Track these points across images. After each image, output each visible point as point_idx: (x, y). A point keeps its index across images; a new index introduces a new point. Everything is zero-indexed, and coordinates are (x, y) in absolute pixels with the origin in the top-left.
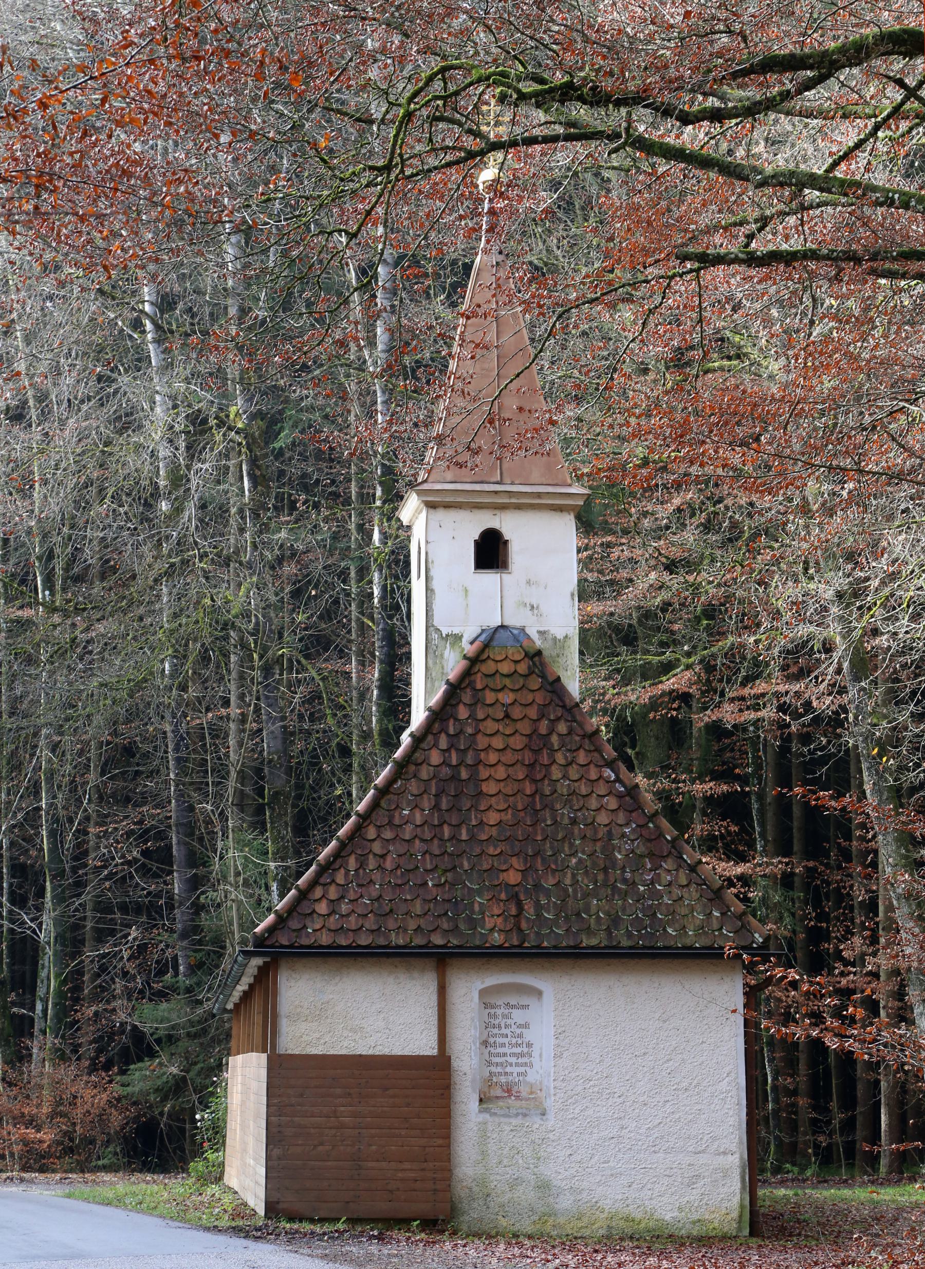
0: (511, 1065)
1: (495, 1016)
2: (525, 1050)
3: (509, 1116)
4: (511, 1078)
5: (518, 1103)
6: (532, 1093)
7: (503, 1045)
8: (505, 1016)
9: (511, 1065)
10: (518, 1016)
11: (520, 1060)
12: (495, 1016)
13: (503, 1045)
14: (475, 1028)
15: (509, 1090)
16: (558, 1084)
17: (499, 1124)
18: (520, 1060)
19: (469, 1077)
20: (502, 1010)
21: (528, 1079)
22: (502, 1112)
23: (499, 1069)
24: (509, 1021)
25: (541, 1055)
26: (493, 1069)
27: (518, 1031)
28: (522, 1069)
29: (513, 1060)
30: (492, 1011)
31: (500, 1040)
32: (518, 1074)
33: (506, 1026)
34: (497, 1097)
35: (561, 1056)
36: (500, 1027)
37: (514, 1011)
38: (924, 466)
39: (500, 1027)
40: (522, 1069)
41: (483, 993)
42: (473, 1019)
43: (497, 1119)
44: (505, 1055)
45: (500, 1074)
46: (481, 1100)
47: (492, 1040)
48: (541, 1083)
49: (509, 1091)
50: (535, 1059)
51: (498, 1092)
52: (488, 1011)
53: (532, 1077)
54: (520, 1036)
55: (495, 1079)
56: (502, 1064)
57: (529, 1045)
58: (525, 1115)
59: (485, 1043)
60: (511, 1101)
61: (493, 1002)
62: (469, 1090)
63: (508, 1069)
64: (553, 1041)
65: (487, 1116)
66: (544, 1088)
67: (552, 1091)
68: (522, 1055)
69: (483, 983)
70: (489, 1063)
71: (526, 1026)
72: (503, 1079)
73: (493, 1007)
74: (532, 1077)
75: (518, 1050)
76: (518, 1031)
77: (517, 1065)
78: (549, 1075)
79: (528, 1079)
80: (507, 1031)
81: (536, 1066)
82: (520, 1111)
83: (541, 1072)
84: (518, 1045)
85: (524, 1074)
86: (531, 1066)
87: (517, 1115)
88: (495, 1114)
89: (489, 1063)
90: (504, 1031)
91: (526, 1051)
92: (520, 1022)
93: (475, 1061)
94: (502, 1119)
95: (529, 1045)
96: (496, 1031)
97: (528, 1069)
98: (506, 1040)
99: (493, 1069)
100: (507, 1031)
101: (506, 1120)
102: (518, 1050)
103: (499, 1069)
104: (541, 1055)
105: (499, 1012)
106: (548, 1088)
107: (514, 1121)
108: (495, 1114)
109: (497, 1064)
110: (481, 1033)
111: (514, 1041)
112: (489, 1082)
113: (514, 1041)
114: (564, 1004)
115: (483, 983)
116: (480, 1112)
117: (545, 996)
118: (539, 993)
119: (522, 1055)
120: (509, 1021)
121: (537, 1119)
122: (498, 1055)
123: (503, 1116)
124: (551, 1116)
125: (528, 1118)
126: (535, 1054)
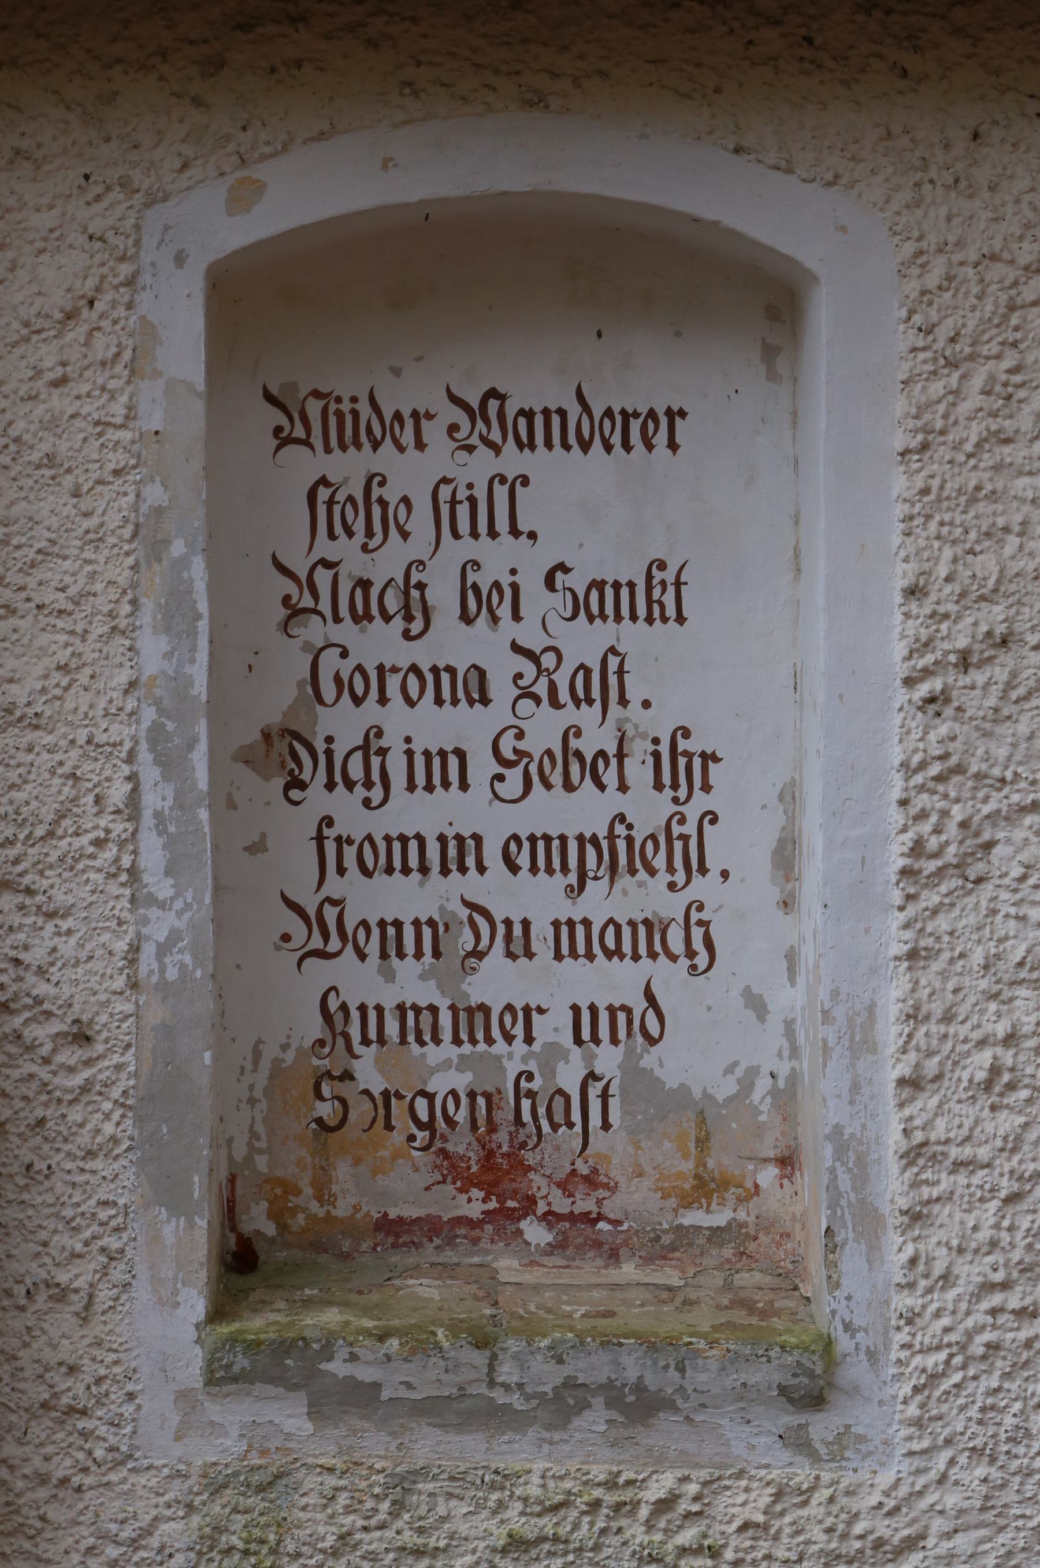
0: (518, 942)
1: (375, 512)
2: (648, 809)
3: (492, 1418)
4: (514, 1058)
5: (581, 1288)
6: (705, 1188)
7: (444, 769)
8: (457, 512)
9: (518, 942)
10: (583, 509)
11: (598, 903)
12: (375, 512)
13: (444, 769)
14: (175, 616)
15: (497, 1165)
16: (948, 1115)
17: (401, 1487)
18: (598, 903)
19: (119, 1065)
20: (439, 458)
21: (673, 1063)
22: (428, 1380)
23: (413, 983)
24: (497, 558)
25: (786, 857)
26: (358, 981)
27: (584, 643)
28: (615, 982)
29: (537, 899)
30: (349, 469)
31: (434, 725)
32: (586, 1025)
33: (477, 602)
34: (393, 1230)
35: (968, 869)
36: (414, 610)
37: (535, 463)
38: (366, 1566)
39: (414, 610)
40: (615, 982)
41: (245, 298)
42: (147, 533)
43: (376, 1446)
44: (461, 853)
45: (418, 1023)
46: (241, 1265)
47: (342, 725)
48: (787, 1097)
49: (499, 1175)
50: (736, 894)
51: (407, 1186)
52: (305, 465)
53: (705, 1048)
54: (603, 684)
55: (369, 1072)
56: (434, 931)
57: (683, 766)
58: (638, 1406)
59: (285, 754)
60: (521, 1266)
61: (347, 384)
62: (120, 1180)
63: (496, 982)
64: (897, 734)
65: (289, 1417)
66: (819, 1158)
67: (892, 1188)
68: (616, 853)
69: (242, 199)
70: (325, 930)
71: (655, 596)
72: (446, 1070)
73: (349, 430)
74: (705, 1048)
75: (584, 812)
76: (584, 643)
77: (572, 940)
78: (862, 1041)
79: (673, 1063)
80: (483, 646)
81: (747, 948)
82: (593, 1367)
83: (786, 999)
84: (578, 766)
85: (641, 1023)
86: (702, 951)
87: (564, 1404)
88: (362, 1397)
89: (325, 930)
90: (454, 644)
91: (653, 831)
92: (604, 556)
93: (175, 917)
94: (427, 1445)
95: (683, 766)
96: (381, 644)
97: (669, 977)
98: (470, 728)
99: (358, 981)
100: (483, 646)
101: (471, 1449)
102: (584, 812)
103: (413, 983)
104: (786, 857)
105: (411, 474)
106: (853, 1151)
107: (536, 1462)
108: (362, 1397)
109: (390, 938)
110: (233, 665)
111: (544, 730)
112: (317, 1093)
113: (544, 730)
114: (1005, 395)
115: (242, 199)
116: (219, 1377)
117: (823, 314)
118: (767, 303)
119: (616, 853)
120: (497, 558)
121: (756, 1445)
122: (402, 855)
123: (431, 1410)
124: (881, 1405)
125: (667, 1432)
126: (740, 843)
